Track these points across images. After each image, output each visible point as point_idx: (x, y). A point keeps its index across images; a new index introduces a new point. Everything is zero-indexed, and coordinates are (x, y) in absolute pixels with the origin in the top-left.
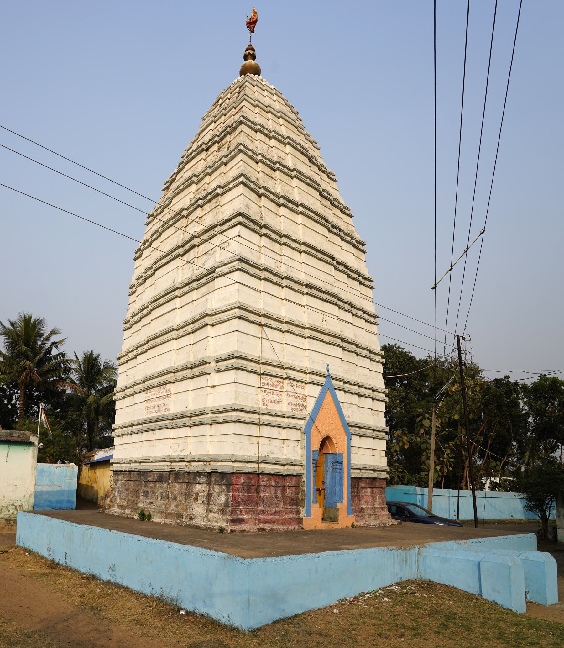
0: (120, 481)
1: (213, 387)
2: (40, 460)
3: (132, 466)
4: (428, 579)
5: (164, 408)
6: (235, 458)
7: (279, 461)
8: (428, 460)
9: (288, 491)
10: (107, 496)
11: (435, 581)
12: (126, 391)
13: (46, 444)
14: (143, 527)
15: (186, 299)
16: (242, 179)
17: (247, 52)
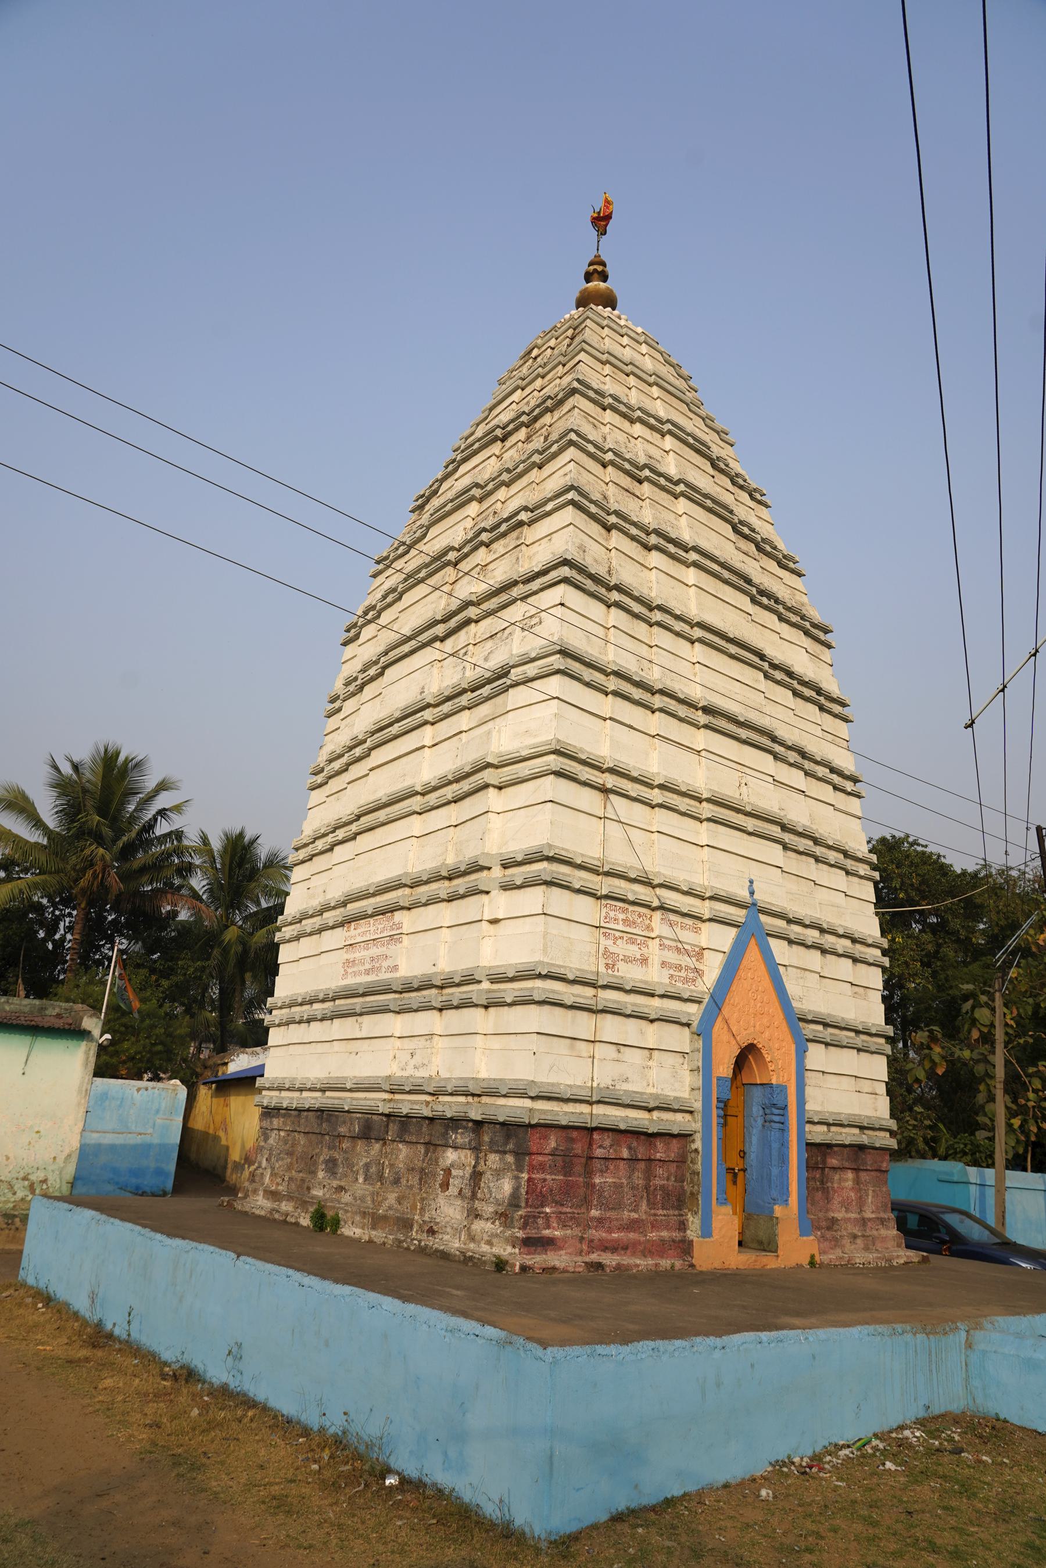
0: (275, 1132)
1: (494, 922)
2: (101, 1071)
3: (304, 1099)
4: (992, 1413)
5: (385, 964)
6: (538, 1090)
7: (638, 1100)
8: (991, 1104)
9: (660, 1171)
10: (248, 1160)
11: (1011, 1421)
12: (304, 922)
13: (121, 1033)
14: (318, 1249)
15: (445, 728)
16: (571, 495)
17: (592, 268)
